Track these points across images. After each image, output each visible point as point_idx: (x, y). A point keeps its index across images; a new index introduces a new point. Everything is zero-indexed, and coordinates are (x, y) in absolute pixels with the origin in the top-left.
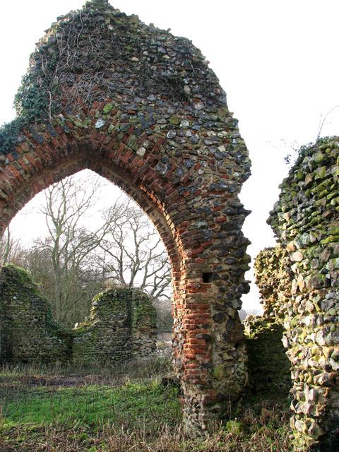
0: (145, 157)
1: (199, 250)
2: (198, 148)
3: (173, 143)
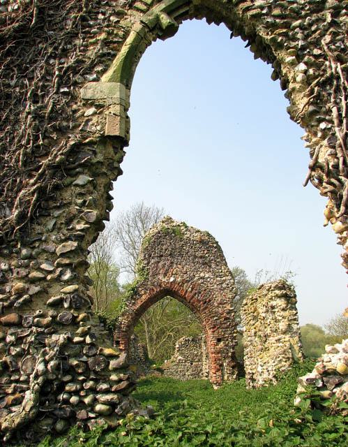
0: (191, 292)
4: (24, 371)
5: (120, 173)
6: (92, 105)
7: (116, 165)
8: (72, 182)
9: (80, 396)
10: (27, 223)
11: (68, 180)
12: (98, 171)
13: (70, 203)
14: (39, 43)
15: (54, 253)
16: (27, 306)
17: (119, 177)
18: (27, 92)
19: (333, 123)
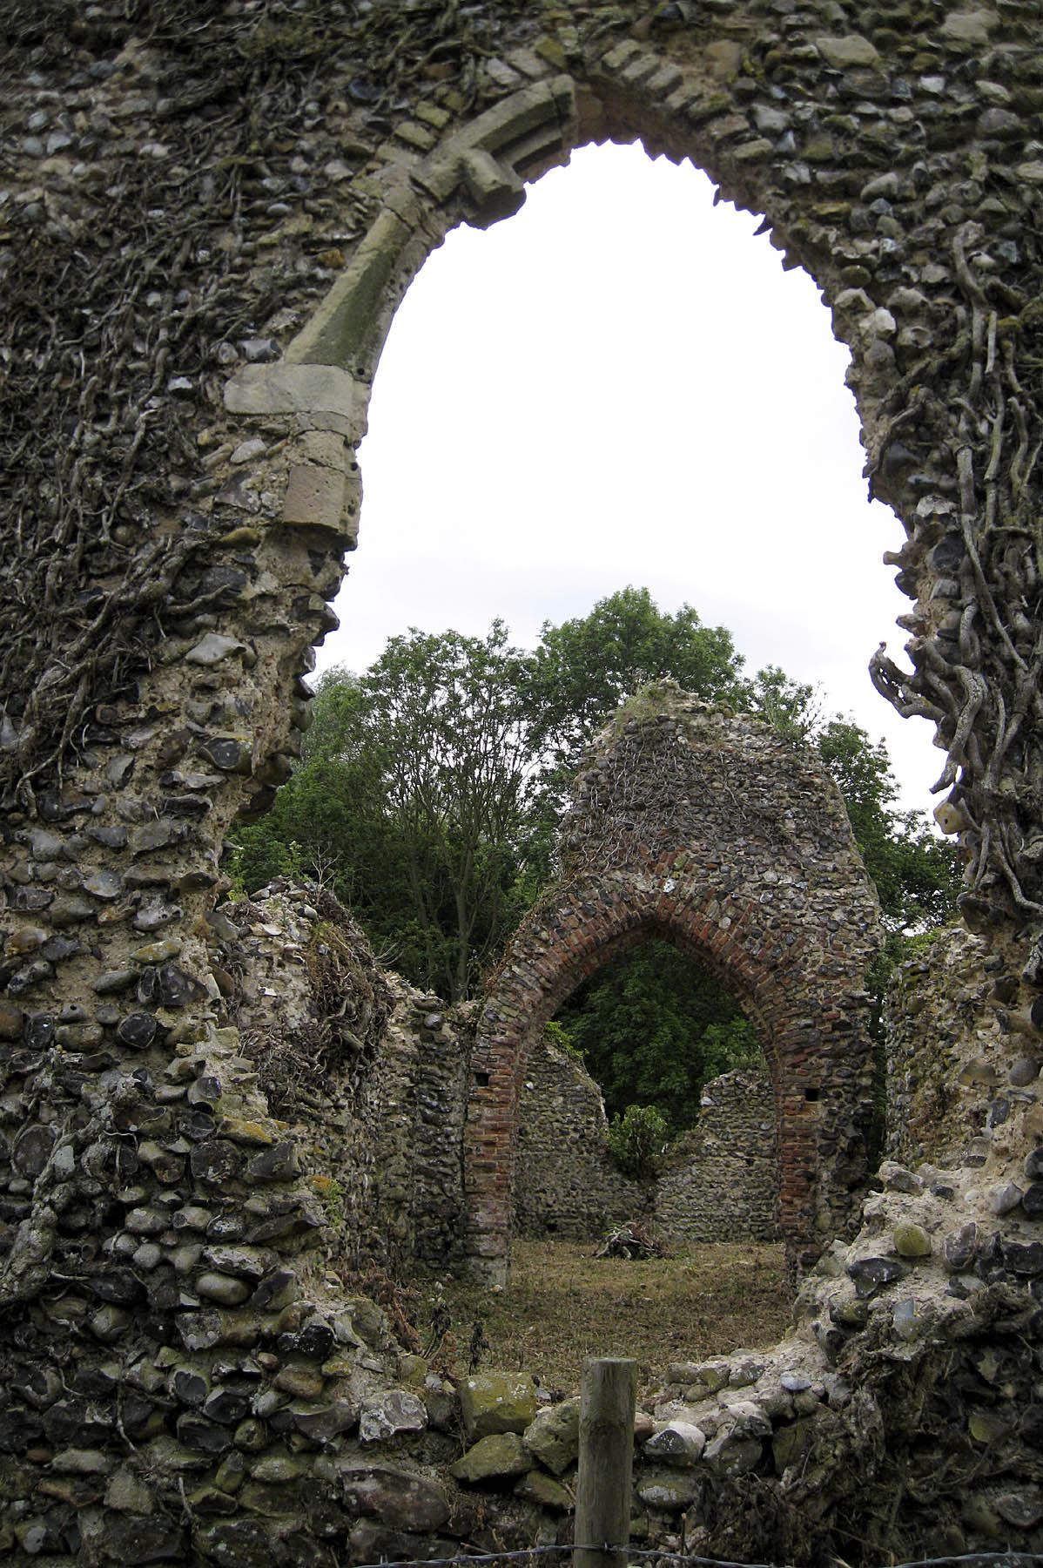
0: (730, 930)
1: (802, 1057)
2: (803, 916)
3: (768, 909)
4: (21, 1166)
5: (331, 624)
6: (253, 429)
7: (315, 603)
8: (183, 654)
9: (164, 1247)
10: (55, 764)
11: (174, 647)
12: (262, 620)
13: (175, 713)
14: (124, 243)
15: (121, 849)
16: (41, 991)
17: (329, 637)
18: (80, 389)
19: (957, 499)
